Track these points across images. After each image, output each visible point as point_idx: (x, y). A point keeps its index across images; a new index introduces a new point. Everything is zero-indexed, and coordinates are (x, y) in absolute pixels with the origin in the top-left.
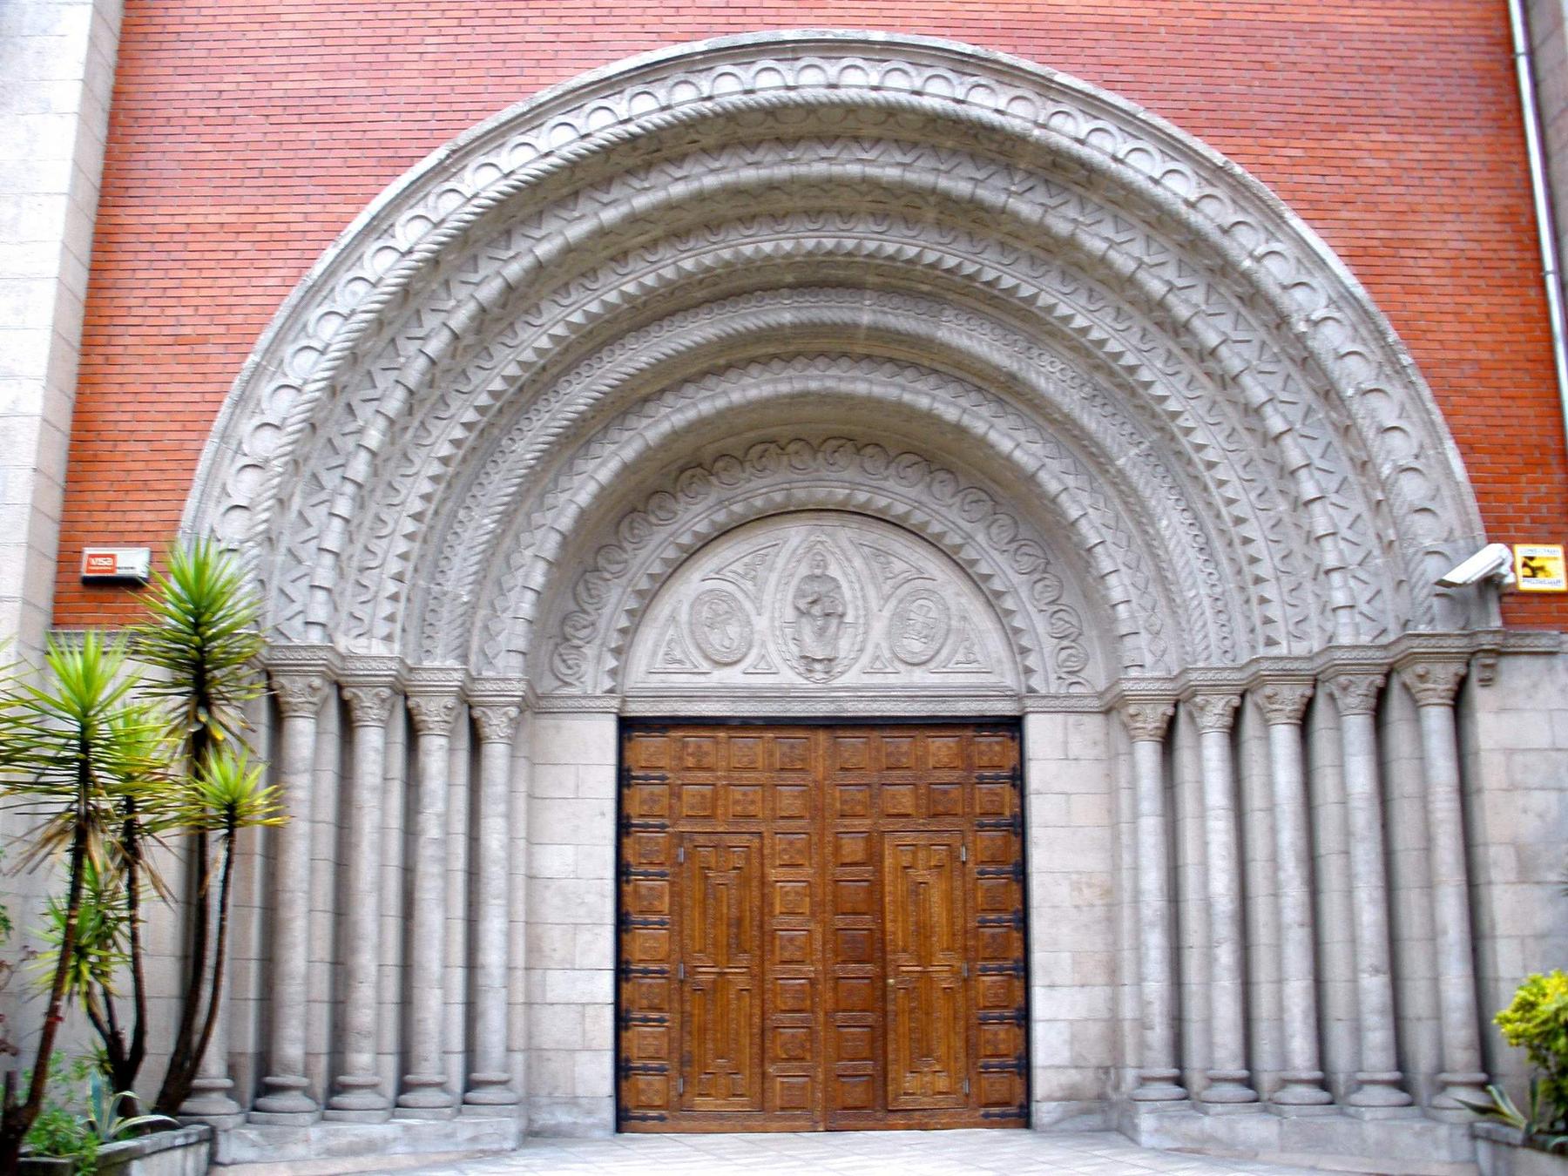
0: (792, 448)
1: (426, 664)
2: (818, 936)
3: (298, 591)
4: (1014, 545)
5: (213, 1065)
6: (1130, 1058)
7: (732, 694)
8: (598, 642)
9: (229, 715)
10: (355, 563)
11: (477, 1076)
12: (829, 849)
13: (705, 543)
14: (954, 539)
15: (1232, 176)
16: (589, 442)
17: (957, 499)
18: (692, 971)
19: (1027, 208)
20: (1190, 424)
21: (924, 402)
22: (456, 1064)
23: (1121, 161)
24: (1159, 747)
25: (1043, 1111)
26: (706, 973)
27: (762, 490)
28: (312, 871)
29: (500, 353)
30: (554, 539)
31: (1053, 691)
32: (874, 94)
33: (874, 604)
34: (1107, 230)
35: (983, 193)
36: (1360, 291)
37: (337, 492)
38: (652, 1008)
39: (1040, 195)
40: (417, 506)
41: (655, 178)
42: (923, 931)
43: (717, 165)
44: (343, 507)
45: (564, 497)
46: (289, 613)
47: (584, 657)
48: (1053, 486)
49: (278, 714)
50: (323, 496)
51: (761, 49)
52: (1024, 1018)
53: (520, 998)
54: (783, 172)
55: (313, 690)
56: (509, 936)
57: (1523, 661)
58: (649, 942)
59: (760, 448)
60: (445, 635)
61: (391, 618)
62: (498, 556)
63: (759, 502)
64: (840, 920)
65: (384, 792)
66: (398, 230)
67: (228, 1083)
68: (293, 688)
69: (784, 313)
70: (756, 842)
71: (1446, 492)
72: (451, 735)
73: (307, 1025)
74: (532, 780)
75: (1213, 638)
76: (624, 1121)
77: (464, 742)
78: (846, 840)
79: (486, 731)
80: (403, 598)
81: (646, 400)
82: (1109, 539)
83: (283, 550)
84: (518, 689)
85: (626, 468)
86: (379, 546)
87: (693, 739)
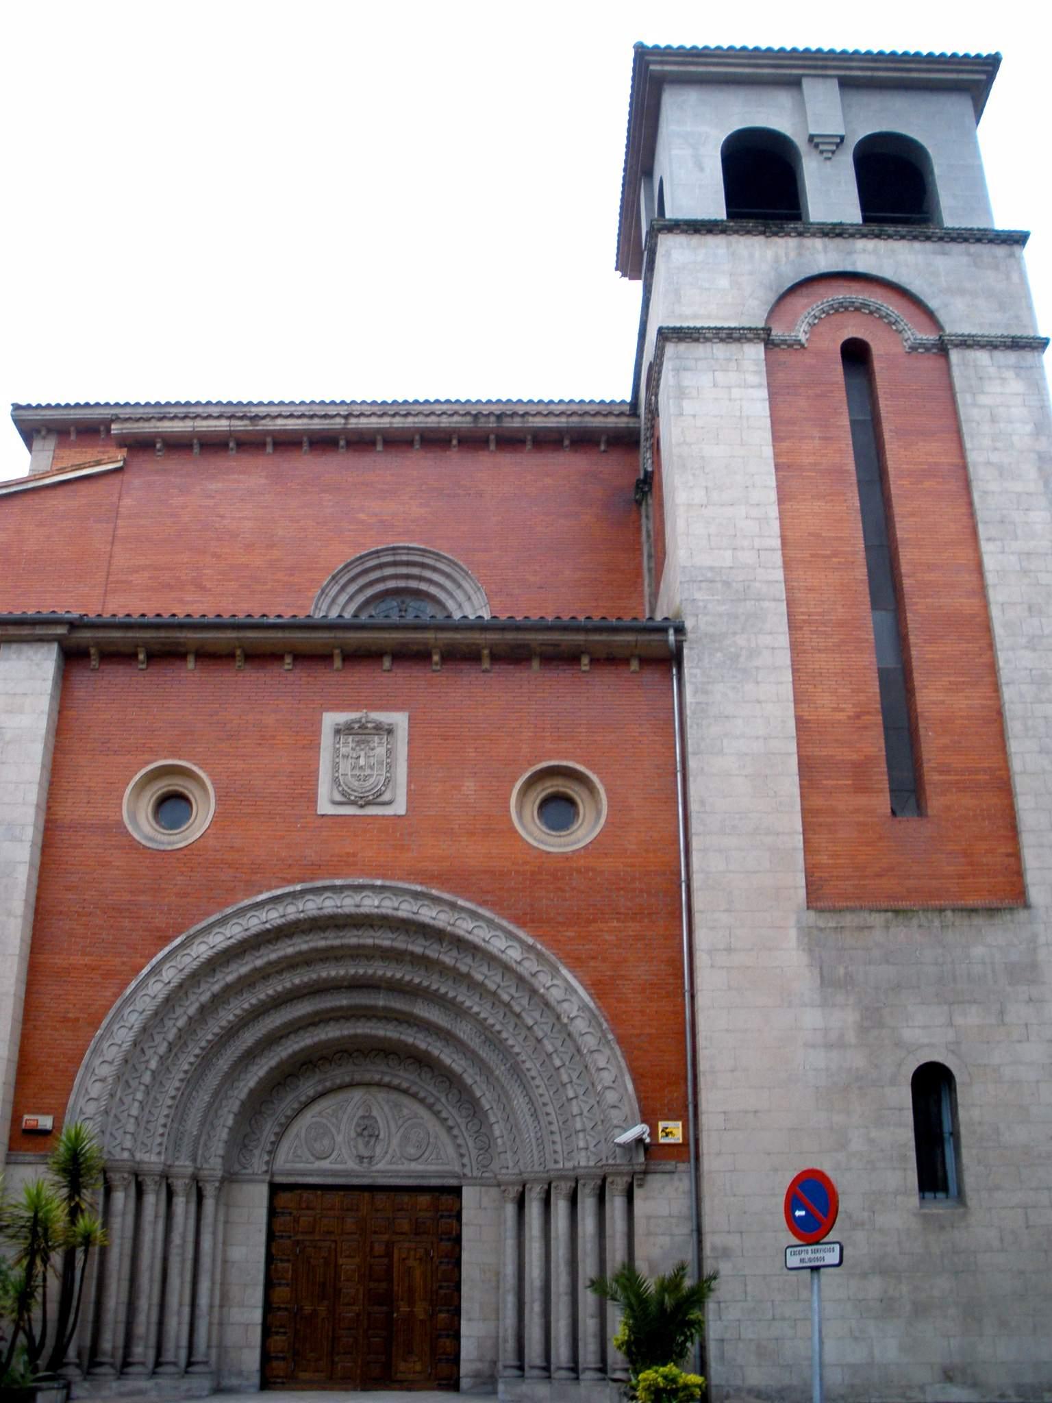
0: (355, 1054)
1: (177, 1163)
2: (361, 1291)
3: (119, 1134)
4: (459, 1104)
5: (72, 1352)
6: (501, 1357)
7: (324, 1173)
8: (260, 1147)
9: (87, 1194)
10: (145, 1119)
11: (193, 1359)
12: (368, 1249)
13: (313, 1100)
14: (431, 1100)
15: (537, 950)
16: (254, 1057)
17: (433, 1081)
18: (301, 1309)
19: (448, 960)
20: (524, 1058)
21: (410, 1040)
22: (183, 1353)
23: (488, 942)
24: (516, 1206)
25: (465, 1383)
26: (308, 1309)
27: (340, 1074)
28: (121, 1260)
29: (211, 1022)
30: (238, 1103)
31: (475, 1174)
32: (376, 910)
33: (393, 1129)
34: (485, 969)
35: (429, 952)
36: (592, 1005)
37: (136, 1090)
38: (281, 1326)
39: (454, 953)
40: (173, 1093)
41: (279, 945)
42: (411, 1290)
43: (308, 938)
44: (139, 1096)
45: (242, 1084)
46: (114, 1144)
47: (254, 1155)
48: (469, 1081)
49: (108, 1191)
50: (130, 1091)
51: (325, 889)
52: (457, 1336)
53: (216, 1321)
54: (337, 942)
55: (124, 1179)
56: (212, 1290)
57: (658, 1176)
58: (282, 1293)
59: (340, 1054)
60: (186, 1149)
61: (160, 1144)
62: (212, 1109)
63: (338, 1081)
64: (372, 1285)
65: (155, 1222)
66: (164, 973)
67: (77, 1361)
68: (116, 1178)
69: (343, 1000)
70: (333, 1246)
71: (625, 1098)
72: (188, 1196)
73: (114, 1334)
74: (227, 1215)
75: (536, 1158)
76: (267, 1383)
77: (194, 1199)
78: (376, 1245)
79: (205, 1193)
80: (166, 1135)
81: (281, 1037)
82: (495, 1107)
83: (112, 1115)
84: (219, 1173)
85: (272, 1069)
86: (156, 1112)
87: (306, 1195)
